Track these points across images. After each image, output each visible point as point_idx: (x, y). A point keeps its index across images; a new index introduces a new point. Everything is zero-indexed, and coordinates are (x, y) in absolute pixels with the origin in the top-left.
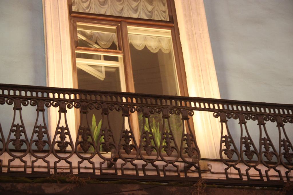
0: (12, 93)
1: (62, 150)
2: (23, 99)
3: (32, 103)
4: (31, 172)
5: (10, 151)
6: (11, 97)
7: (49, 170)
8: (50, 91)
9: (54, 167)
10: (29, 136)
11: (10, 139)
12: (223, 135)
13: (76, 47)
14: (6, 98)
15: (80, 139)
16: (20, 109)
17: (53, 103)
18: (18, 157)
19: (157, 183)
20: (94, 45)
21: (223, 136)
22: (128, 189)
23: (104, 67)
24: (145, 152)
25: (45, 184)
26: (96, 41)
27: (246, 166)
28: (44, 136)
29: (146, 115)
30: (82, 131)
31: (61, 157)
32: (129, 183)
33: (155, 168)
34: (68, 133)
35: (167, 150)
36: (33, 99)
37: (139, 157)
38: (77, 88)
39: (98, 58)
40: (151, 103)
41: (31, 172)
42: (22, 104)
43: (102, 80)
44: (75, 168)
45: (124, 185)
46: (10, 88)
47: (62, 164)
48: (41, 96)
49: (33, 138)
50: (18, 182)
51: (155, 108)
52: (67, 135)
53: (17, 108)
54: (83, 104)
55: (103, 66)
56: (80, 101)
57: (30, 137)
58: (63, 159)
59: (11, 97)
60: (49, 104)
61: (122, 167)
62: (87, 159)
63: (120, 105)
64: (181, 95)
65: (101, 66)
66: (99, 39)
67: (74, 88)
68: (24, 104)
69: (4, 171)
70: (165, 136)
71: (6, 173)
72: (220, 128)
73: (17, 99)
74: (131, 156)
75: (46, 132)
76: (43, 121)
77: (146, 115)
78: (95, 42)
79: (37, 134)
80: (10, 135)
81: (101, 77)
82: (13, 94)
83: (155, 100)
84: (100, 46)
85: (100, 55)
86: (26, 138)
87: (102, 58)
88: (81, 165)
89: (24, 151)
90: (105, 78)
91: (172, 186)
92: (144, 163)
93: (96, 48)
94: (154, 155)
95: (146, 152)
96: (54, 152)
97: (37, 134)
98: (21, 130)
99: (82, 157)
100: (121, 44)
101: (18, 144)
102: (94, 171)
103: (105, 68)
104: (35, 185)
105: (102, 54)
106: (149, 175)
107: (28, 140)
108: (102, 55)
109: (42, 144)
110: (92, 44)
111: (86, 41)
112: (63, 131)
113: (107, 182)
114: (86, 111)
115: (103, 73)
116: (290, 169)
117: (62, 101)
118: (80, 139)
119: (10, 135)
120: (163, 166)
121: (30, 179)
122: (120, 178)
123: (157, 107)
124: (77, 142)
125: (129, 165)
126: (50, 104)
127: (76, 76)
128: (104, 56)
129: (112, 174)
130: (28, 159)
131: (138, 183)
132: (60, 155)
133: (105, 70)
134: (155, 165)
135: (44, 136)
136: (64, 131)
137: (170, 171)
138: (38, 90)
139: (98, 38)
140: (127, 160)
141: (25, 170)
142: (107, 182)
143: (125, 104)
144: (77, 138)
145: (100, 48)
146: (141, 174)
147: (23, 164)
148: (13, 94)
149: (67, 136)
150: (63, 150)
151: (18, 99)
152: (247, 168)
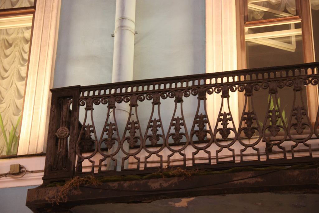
0: (225, 80)
1: (225, 138)
2: (102, 98)
3: (240, 90)
4: (239, 162)
5: (193, 144)
6: (151, 92)
7: (259, 158)
8: (167, 81)
9: (208, 158)
10: (121, 133)
11: (217, 129)
12: (175, 117)
13: (245, 23)
14: (214, 87)
15: (244, 125)
16: (158, 103)
17: (169, 94)
18: (225, 147)
19: (279, 167)
20: (281, 13)
21: (175, 118)
22: (239, 178)
23: (295, 37)
24: (295, 131)
25: (151, 180)
26: (285, 8)
27: (101, 156)
28: (181, 128)
29: (272, 91)
30: (199, 119)
31: (247, 145)
32: (241, 171)
33: (282, 150)
34: (231, 119)
35: (297, 128)
36: (171, 91)
37: (288, 138)
38: (244, 67)
39: (287, 27)
40: (281, 75)
41: (143, 169)
42: (161, 98)
43: (294, 51)
44: (189, 159)
45: (237, 174)
46: (84, 90)
47: (226, 152)
48: (198, 85)
49: (218, 126)
50: (125, 180)
51: (285, 81)
52: (182, 125)
53: (111, 106)
54: (201, 90)
55: (293, 36)
56: (197, 88)
57: (123, 133)
58: (176, 151)
59: (151, 92)
60: (187, 93)
61: (292, 149)
62: (202, 148)
63: (242, 84)
64: (316, 61)
65: (291, 36)
66: (289, 6)
67: (133, 80)
68: (141, 100)
69: (237, 160)
70: (271, 114)
71: (265, 161)
72: (243, 101)
73: (111, 98)
74: (303, 136)
75: (305, 114)
76: (181, 114)
77: (272, 91)
78: (284, 10)
79: (174, 127)
80: (170, 128)
81: (292, 48)
82: (244, 80)
83: (286, 71)
84: (291, 14)
85: (290, 24)
86: (186, 131)
87: (293, 26)
88: (196, 156)
89: (160, 145)
90: (296, 49)
91: (295, 169)
92: (294, 143)
93: (286, 17)
94: (281, 135)
95: (297, 131)
96: (168, 145)
97: (174, 127)
98: (278, 115)
99: (197, 147)
100: (299, 8)
101: (132, 142)
102: (210, 161)
103: (296, 38)
104: (141, 182)
105: (292, 22)
106: (272, 158)
107: (164, 134)
108: (293, 24)
109: (201, 134)
110: (278, 14)
111: (269, 12)
112: (224, 118)
113: (218, 172)
114: (203, 97)
115: (293, 44)
116: (111, 156)
117: (178, 91)
118: (244, 125)
119: (170, 128)
120: (292, 146)
121: (140, 176)
122: (264, 164)
123: (288, 80)
124: (240, 130)
125: (301, 146)
126: (308, 81)
127: (244, 55)
128: (296, 24)
129: (198, 165)
130: (165, 153)
131: (252, 170)
132: (173, 148)
133: (296, 39)
134: (281, 146)
135: (181, 128)
136: (179, 121)
137: (299, 151)
138: (155, 83)
139: (287, 4)
140: (272, 143)
141: (161, 165)
142: (219, 171)
143: (248, 83)
144: (240, 124)
145: (291, 15)
146: (289, 157)
147: (182, 157)
148: (244, 80)
149: (182, 127)
150: (177, 142)
151: (134, 95)
152: (101, 158)
